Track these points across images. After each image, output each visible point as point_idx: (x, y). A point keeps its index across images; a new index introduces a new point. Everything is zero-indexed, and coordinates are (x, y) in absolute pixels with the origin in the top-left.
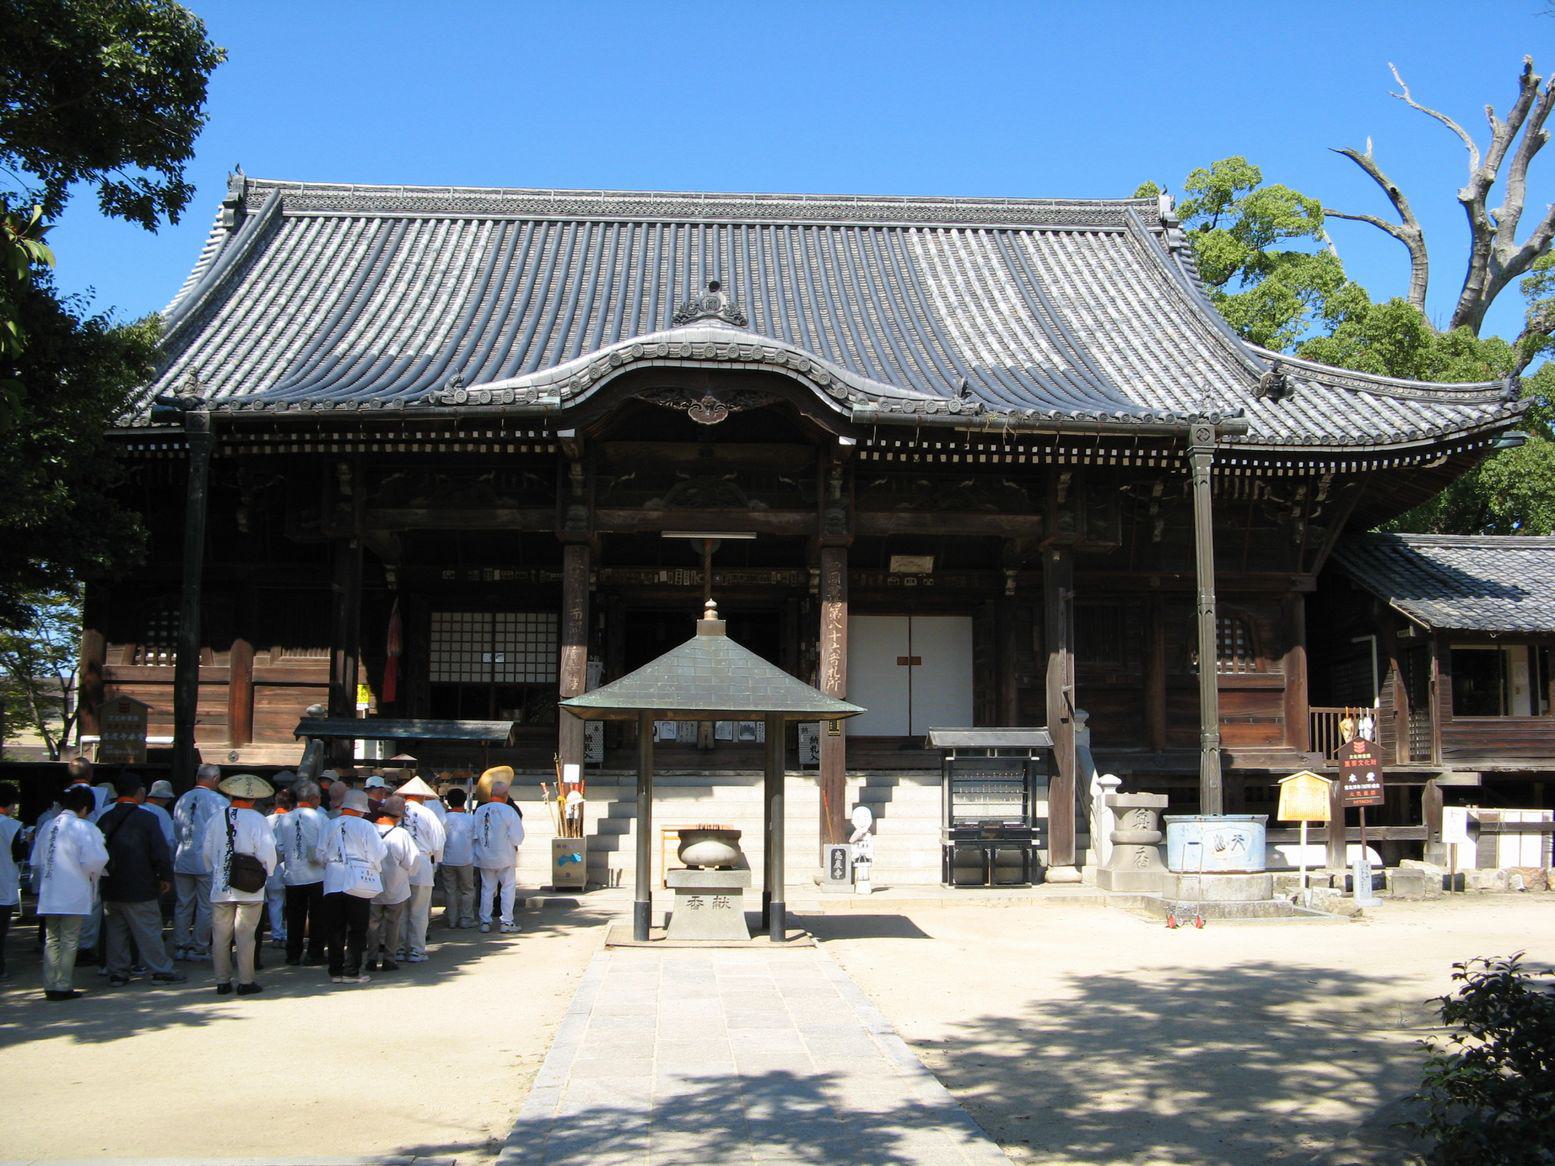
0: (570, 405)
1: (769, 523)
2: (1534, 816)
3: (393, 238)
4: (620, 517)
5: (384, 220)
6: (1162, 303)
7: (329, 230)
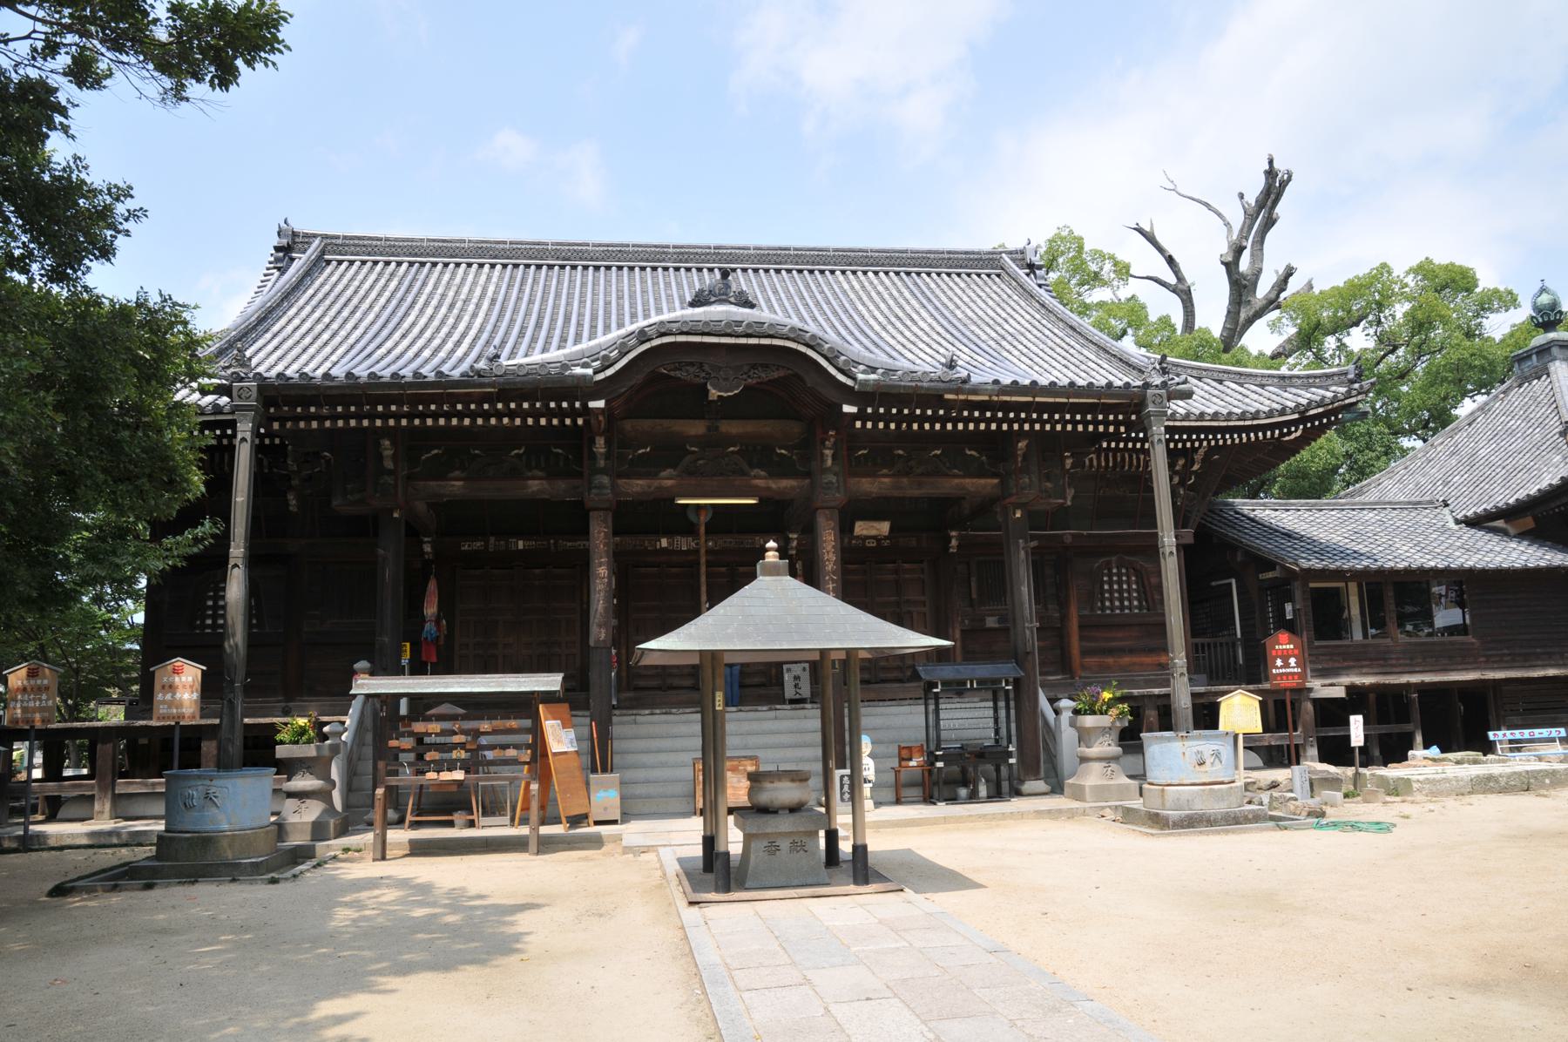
0: (601, 376)
1: (769, 488)
2: (1555, 732)
4: (638, 485)
5: (411, 264)
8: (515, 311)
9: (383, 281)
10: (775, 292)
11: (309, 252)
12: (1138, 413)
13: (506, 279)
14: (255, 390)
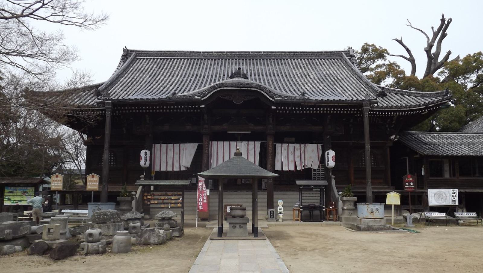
0: (203, 99)
3: (164, 63)
4: (217, 128)
5: (161, 59)
6: (351, 75)
7: (147, 61)
8: (190, 74)
9: (152, 65)
10: (268, 66)
11: (132, 56)
12: (361, 108)
13: (188, 64)
14: (111, 103)
